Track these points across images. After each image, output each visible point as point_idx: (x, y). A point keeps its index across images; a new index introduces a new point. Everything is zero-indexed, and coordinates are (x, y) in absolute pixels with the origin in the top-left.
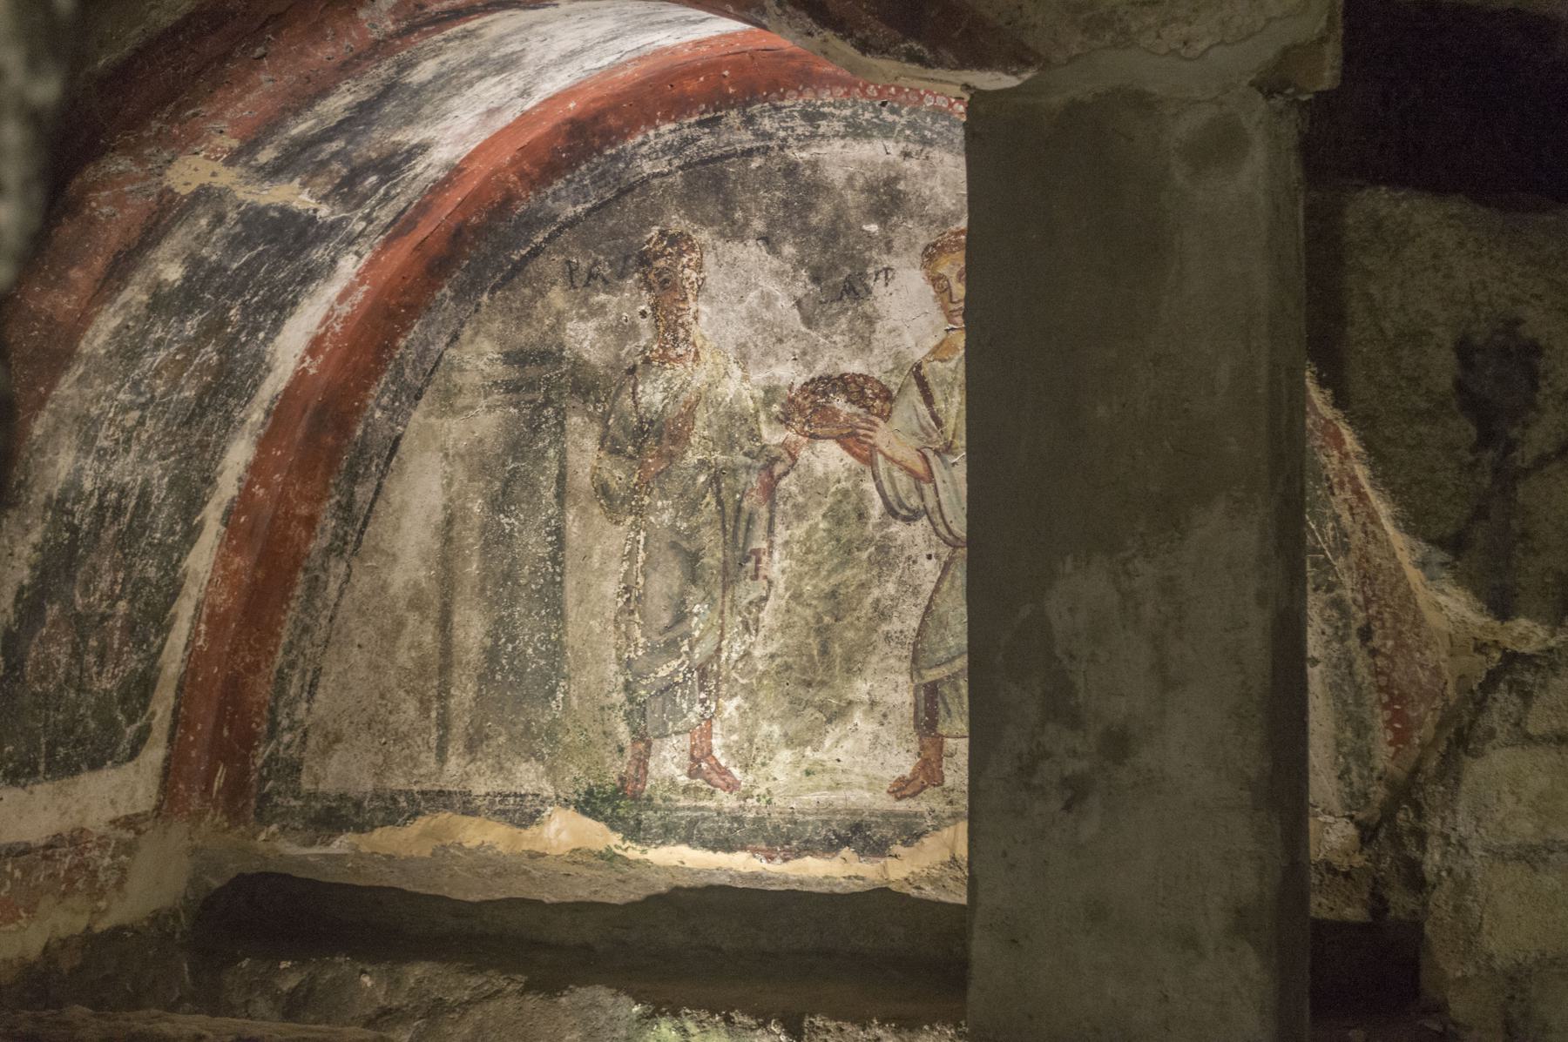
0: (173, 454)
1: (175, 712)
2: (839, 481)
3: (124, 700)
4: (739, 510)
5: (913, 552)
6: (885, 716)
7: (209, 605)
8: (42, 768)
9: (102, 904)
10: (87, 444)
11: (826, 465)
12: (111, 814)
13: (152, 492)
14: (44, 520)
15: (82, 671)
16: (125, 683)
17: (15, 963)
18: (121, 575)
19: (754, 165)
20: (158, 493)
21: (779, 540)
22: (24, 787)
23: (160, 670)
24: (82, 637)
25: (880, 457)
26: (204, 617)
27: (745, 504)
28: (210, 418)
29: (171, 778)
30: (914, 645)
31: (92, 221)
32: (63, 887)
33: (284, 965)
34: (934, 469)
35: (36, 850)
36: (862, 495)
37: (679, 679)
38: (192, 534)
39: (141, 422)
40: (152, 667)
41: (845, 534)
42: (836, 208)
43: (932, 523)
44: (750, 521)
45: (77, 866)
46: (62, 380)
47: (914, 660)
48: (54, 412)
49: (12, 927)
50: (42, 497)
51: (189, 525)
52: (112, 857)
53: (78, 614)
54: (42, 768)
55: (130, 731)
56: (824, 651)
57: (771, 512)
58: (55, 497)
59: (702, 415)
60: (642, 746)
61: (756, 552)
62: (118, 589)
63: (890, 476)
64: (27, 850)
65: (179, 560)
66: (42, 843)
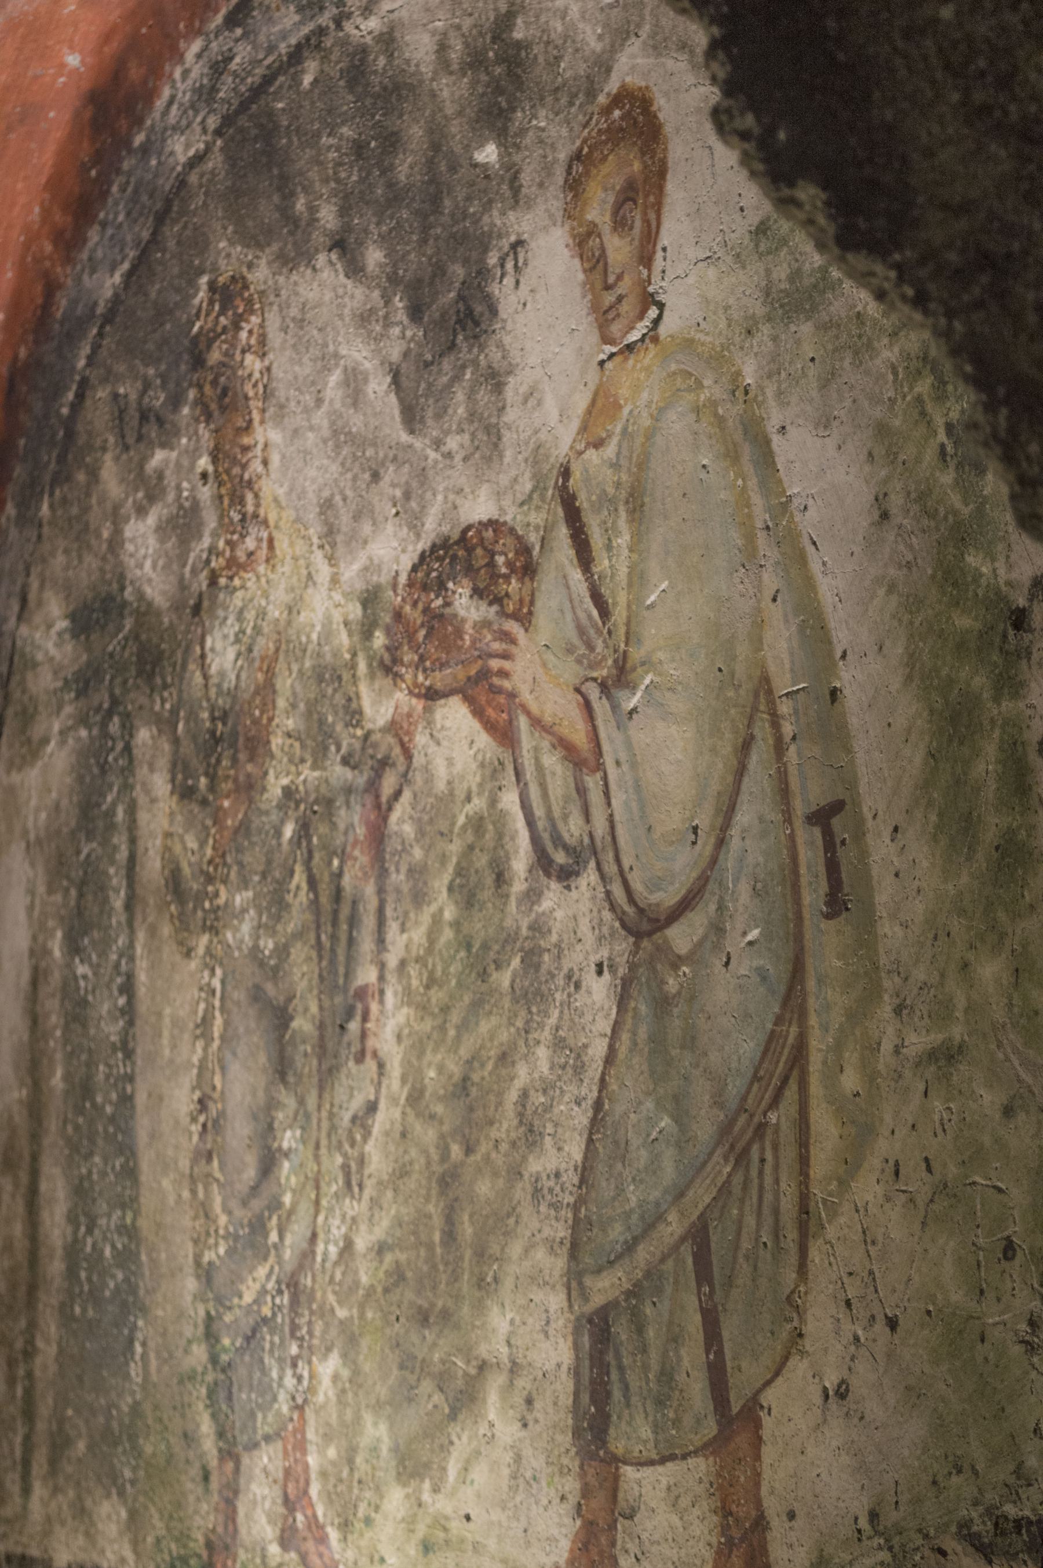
2: (468, 799)
4: (338, 895)
5: (573, 959)
6: (529, 1402)
11: (450, 762)
19: (307, 80)
21: (392, 960)
25: (523, 722)
27: (346, 881)
30: (576, 1208)
34: (603, 734)
36: (501, 819)
37: (266, 1311)
41: (478, 928)
42: (430, 132)
43: (603, 877)
44: (353, 921)
47: (574, 1250)
56: (450, 1236)
57: (381, 891)
59: (286, 683)
60: (230, 1465)
61: (362, 993)
63: (539, 767)
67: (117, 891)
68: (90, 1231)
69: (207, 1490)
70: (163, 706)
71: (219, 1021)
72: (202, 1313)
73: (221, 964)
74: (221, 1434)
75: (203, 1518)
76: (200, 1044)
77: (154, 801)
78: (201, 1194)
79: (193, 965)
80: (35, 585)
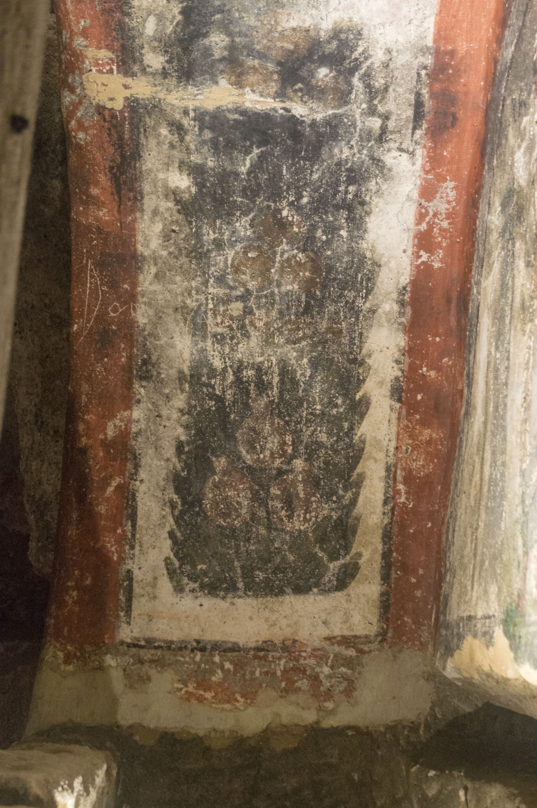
0: (303, 338)
1: (386, 556)
3: (322, 540)
7: (404, 469)
8: (241, 585)
9: (330, 705)
10: (198, 329)
12: (326, 632)
13: (295, 371)
14: (182, 391)
15: (268, 513)
16: (318, 527)
17: (227, 734)
18: (288, 439)
20: (303, 369)
22: (224, 598)
23: (358, 519)
24: (261, 485)
26: (399, 478)
28: (332, 308)
29: (392, 610)
31: (79, 147)
32: (283, 684)
33: (432, 773)
35: (247, 650)
38: (359, 408)
39: (248, 311)
40: (348, 515)
45: (292, 669)
46: (141, 278)
48: (149, 304)
49: (227, 706)
50: (173, 373)
51: (352, 400)
52: (332, 668)
53: (249, 467)
54: (241, 585)
55: (334, 566)
58: (187, 372)
62: (290, 450)
64: (235, 648)
65: (351, 428)
66: (253, 645)
67: (507, 316)
68: (495, 470)
69: (519, 571)
70: (522, 230)
71: (531, 361)
72: (521, 492)
73: (534, 335)
74: (524, 545)
75: (517, 585)
76: (526, 372)
77: (519, 272)
78: (523, 439)
79: (526, 338)
80: (492, 195)
